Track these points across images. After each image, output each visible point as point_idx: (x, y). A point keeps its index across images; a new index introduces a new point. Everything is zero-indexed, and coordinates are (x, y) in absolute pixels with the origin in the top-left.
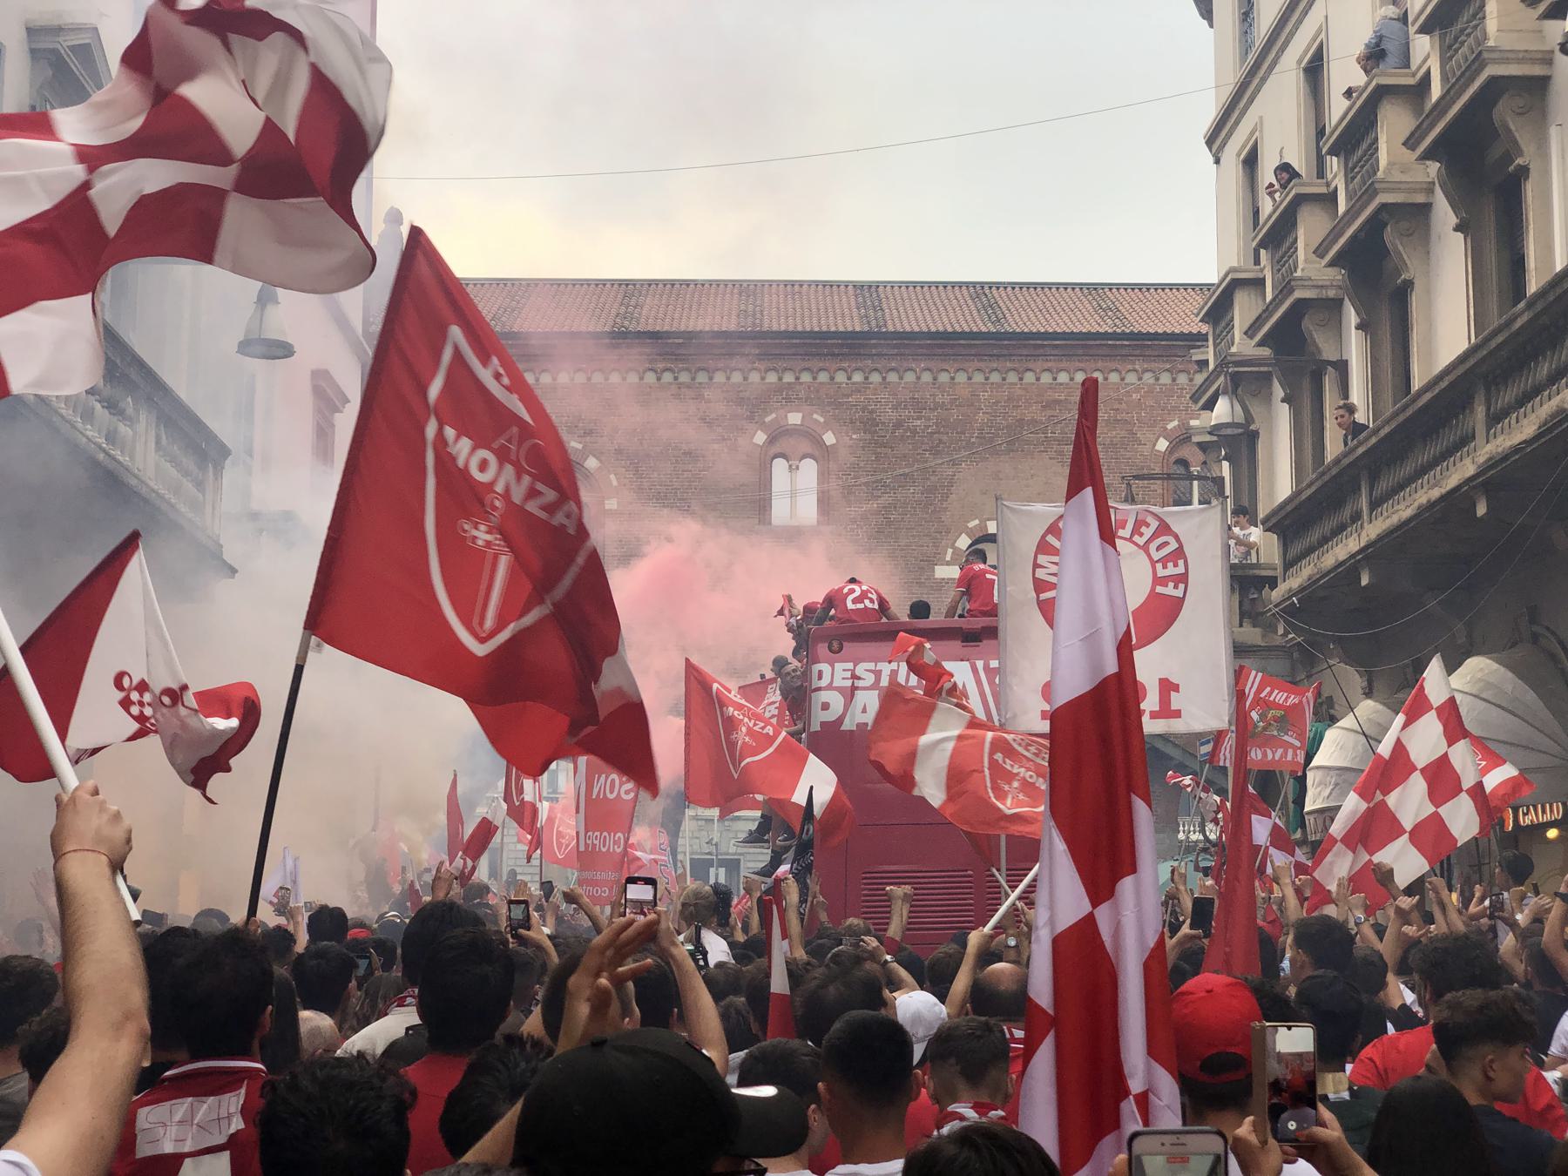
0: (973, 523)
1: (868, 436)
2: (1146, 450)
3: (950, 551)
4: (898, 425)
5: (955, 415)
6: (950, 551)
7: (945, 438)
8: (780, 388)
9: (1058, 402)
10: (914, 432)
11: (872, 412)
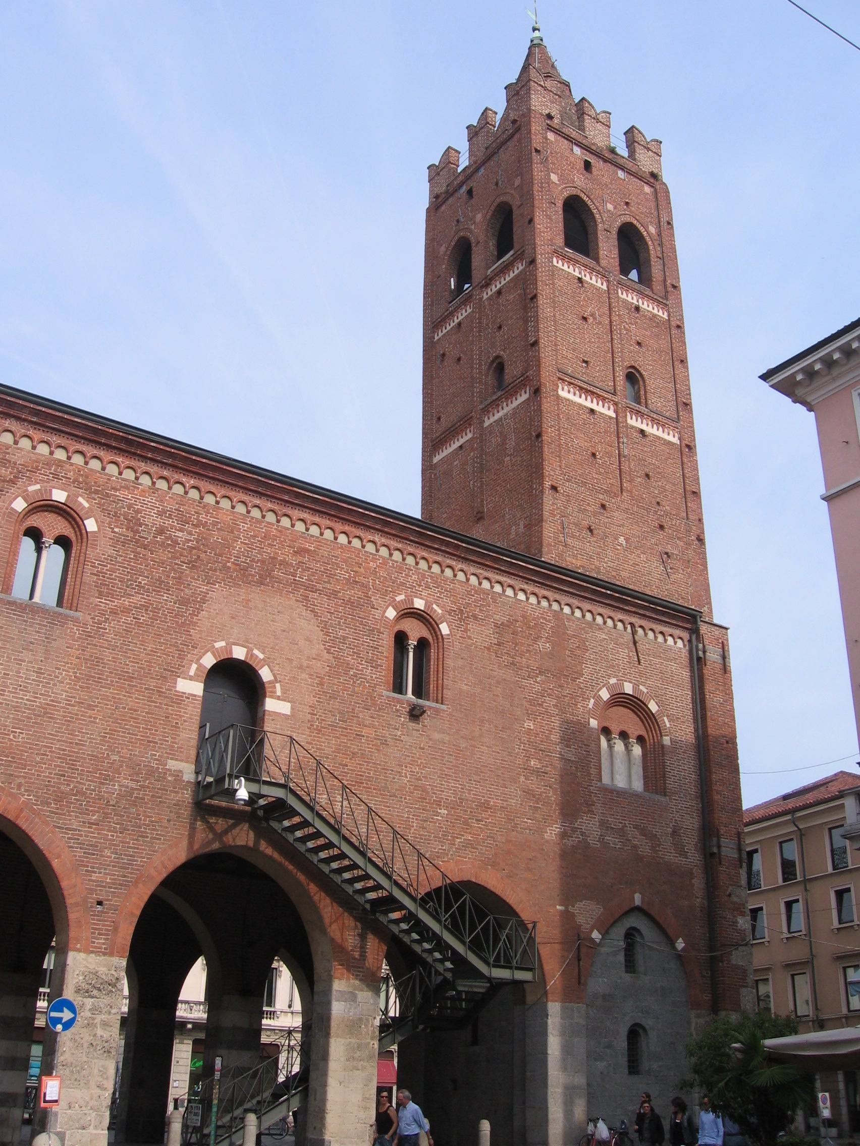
0: (220, 644)
1: (130, 534)
2: (377, 614)
3: (194, 666)
4: (161, 531)
5: (216, 537)
6: (194, 666)
7: (203, 556)
8: (50, 462)
9: (307, 551)
11: (138, 511)
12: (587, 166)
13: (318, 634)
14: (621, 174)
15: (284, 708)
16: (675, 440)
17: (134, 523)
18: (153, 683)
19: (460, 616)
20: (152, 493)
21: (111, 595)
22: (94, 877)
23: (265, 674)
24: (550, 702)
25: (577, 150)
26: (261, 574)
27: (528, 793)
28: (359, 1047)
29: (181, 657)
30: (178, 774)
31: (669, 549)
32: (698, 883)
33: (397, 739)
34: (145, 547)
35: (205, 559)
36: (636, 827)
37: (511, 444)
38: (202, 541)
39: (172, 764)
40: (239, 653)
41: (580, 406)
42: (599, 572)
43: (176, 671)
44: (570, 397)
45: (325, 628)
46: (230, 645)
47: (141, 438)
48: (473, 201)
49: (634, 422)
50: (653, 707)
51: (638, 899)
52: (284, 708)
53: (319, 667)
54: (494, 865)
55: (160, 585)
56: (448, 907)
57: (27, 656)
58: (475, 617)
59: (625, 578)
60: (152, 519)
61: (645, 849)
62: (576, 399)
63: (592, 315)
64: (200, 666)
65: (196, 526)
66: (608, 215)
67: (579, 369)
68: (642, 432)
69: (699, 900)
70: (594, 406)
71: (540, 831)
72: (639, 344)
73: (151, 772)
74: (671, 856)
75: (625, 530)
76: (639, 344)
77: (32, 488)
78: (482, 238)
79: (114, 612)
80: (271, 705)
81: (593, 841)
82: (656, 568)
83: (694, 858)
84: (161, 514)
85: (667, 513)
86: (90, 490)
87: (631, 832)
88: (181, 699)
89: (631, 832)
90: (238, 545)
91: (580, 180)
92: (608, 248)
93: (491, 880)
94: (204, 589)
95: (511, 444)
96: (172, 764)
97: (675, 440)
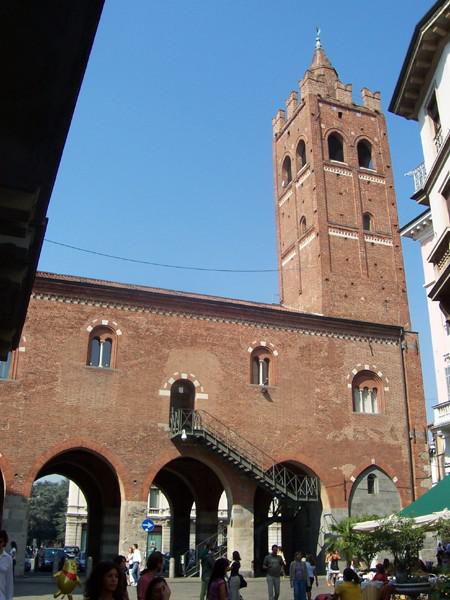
0: (176, 374)
5: (171, 329)
10: (154, 334)
12: (340, 114)
13: (218, 363)
14: (359, 115)
15: (205, 396)
16: (391, 245)
17: (136, 329)
18: (149, 393)
19: (282, 346)
20: (142, 317)
21: (130, 359)
22: (133, 471)
23: (196, 383)
24: (327, 379)
25: (335, 108)
26: (193, 342)
27: (319, 420)
28: (245, 531)
29: (161, 381)
30: (163, 428)
31: (388, 299)
32: (405, 451)
33: (256, 404)
34: (142, 338)
35: (168, 340)
36: (372, 430)
37: (310, 258)
38: (165, 332)
39: (160, 425)
40: (184, 376)
41: (340, 238)
42: (351, 315)
43: (160, 387)
44: (335, 234)
45: (221, 360)
46: (180, 373)
47: (408, 587)
48: (291, 138)
49: (369, 240)
50: (380, 374)
51: (373, 462)
52: (205, 396)
53: (220, 377)
54: (303, 452)
55: (149, 353)
56: (287, 481)
57: (98, 389)
58: (290, 346)
59: (365, 317)
60: (144, 326)
61: (376, 438)
62: (338, 234)
63: (345, 191)
64: (169, 384)
65: (163, 325)
66: (350, 138)
67: (340, 221)
68: (373, 244)
69: (406, 459)
70: (347, 236)
71: (325, 436)
72: (370, 200)
73: (152, 429)
74: (391, 441)
75: (364, 293)
76: (370, 200)
77: (95, 321)
78: (295, 157)
79: (131, 367)
80: (198, 396)
81: (350, 438)
82: (381, 308)
83: (402, 441)
84: (147, 323)
85: (386, 282)
86: (117, 318)
87: (369, 433)
88: (161, 398)
89: (369, 433)
90: (181, 331)
91: (336, 124)
92: (350, 155)
93: (303, 459)
94: (168, 351)
95: (310, 258)
96: (160, 425)
97: (391, 245)
